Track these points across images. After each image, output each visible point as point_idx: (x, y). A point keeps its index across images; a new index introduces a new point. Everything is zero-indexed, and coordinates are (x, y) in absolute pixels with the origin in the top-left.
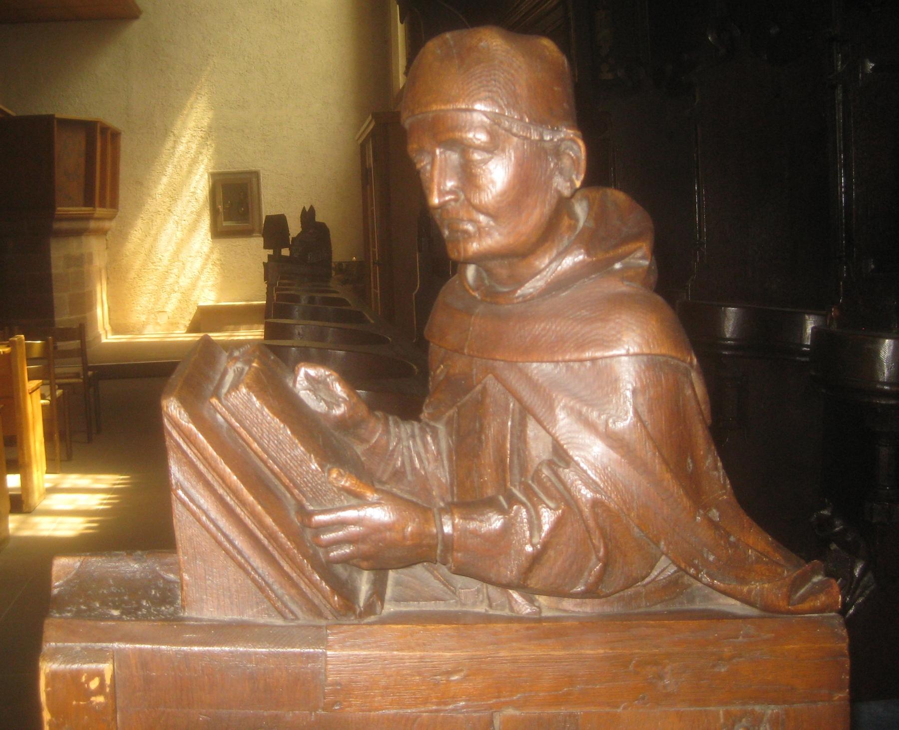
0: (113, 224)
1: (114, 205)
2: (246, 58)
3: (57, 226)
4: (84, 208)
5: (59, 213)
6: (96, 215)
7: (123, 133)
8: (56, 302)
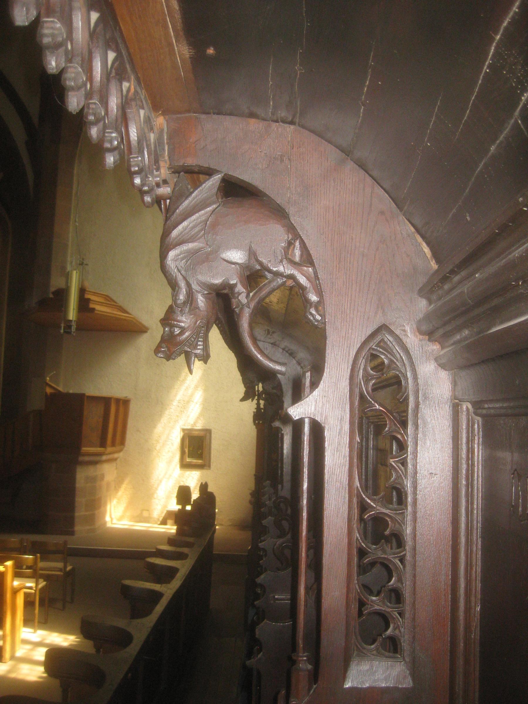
0: (121, 454)
1: (123, 442)
3: (81, 458)
4: (99, 449)
5: (83, 451)
6: (106, 453)
7: (132, 400)
8: (77, 504)
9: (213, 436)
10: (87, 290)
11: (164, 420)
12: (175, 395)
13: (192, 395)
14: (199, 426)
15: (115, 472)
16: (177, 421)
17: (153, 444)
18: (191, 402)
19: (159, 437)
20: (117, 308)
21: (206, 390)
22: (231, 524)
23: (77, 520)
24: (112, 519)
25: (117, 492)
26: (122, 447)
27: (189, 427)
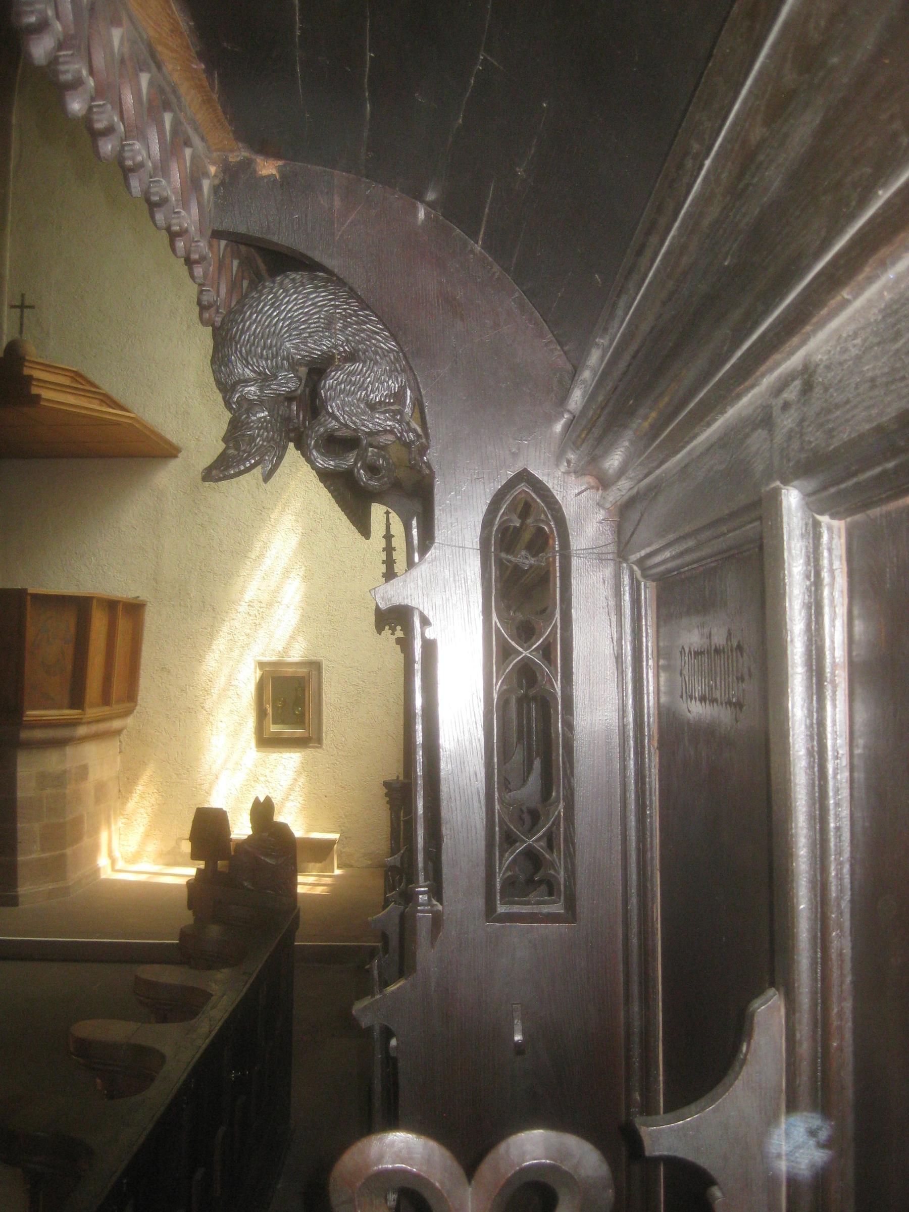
0: (130, 721)
1: (131, 695)
2: (311, 513)
3: (25, 735)
6: (84, 720)
7: (149, 604)
8: (20, 836)
9: (325, 675)
10: (27, 358)
11: (220, 644)
12: (242, 592)
14: (296, 655)
15: (119, 759)
18: (276, 604)
19: (210, 681)
20: (99, 399)
21: (308, 578)
22: (369, 862)
23: (22, 872)
24: (113, 861)
25: (124, 804)
26: (132, 704)
27: (274, 658)
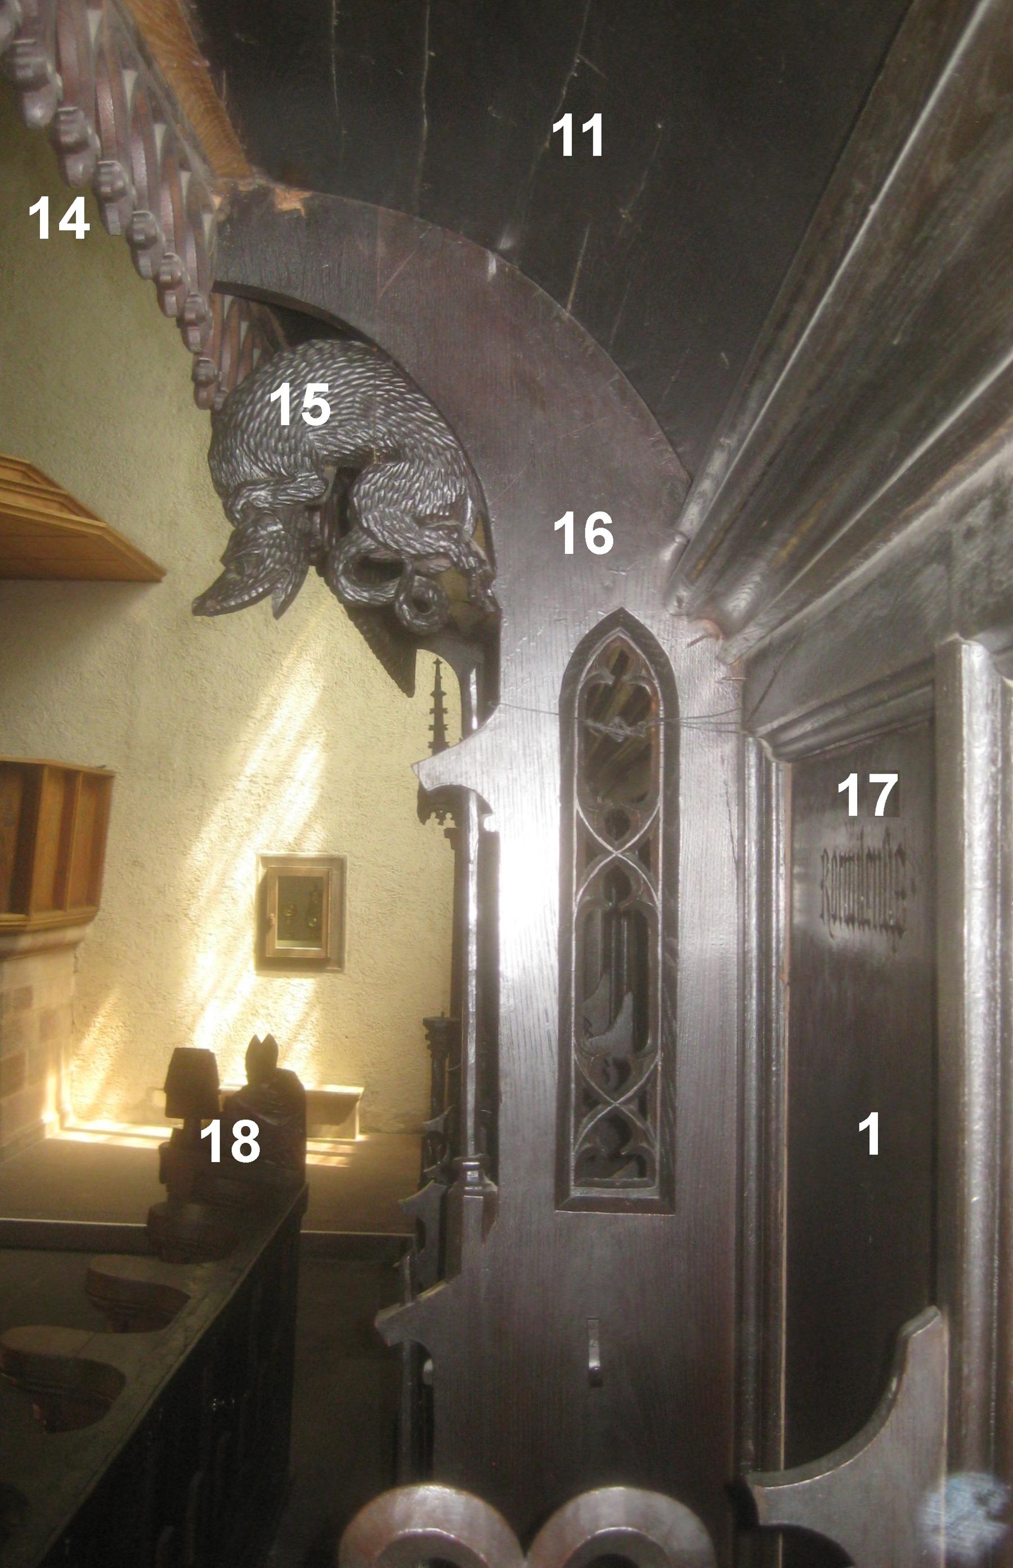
0: (89, 930)
1: (92, 897)
6: (28, 928)
7: (118, 777)
11: (211, 831)
13: (291, 758)
14: (312, 848)
15: (73, 980)
16: (248, 833)
17: (178, 900)
21: (331, 746)
22: (402, 1126)
24: (63, 1116)
25: (79, 1040)
26: (94, 908)
27: (283, 852)
